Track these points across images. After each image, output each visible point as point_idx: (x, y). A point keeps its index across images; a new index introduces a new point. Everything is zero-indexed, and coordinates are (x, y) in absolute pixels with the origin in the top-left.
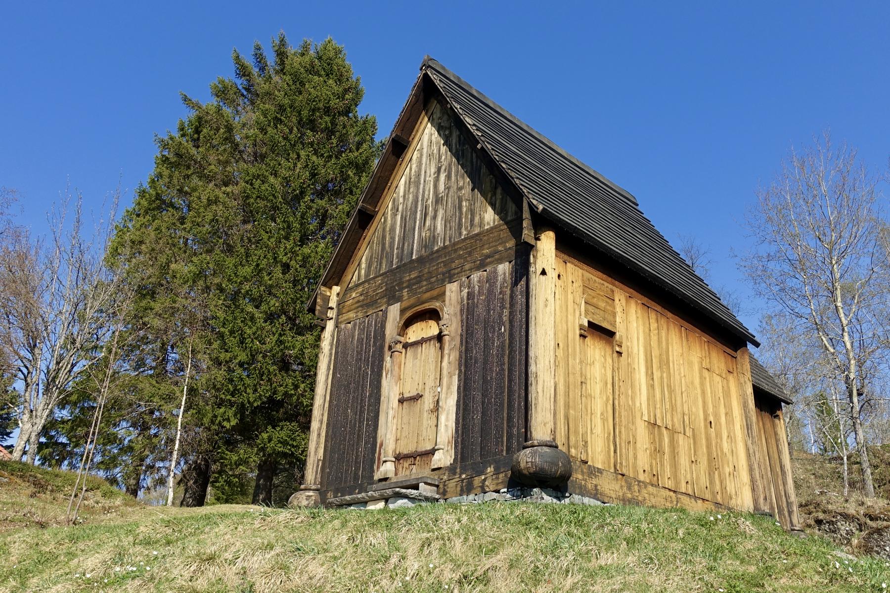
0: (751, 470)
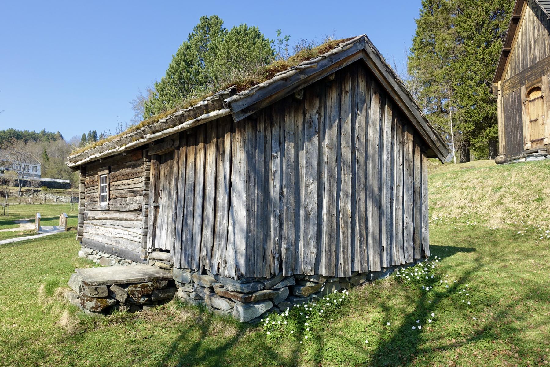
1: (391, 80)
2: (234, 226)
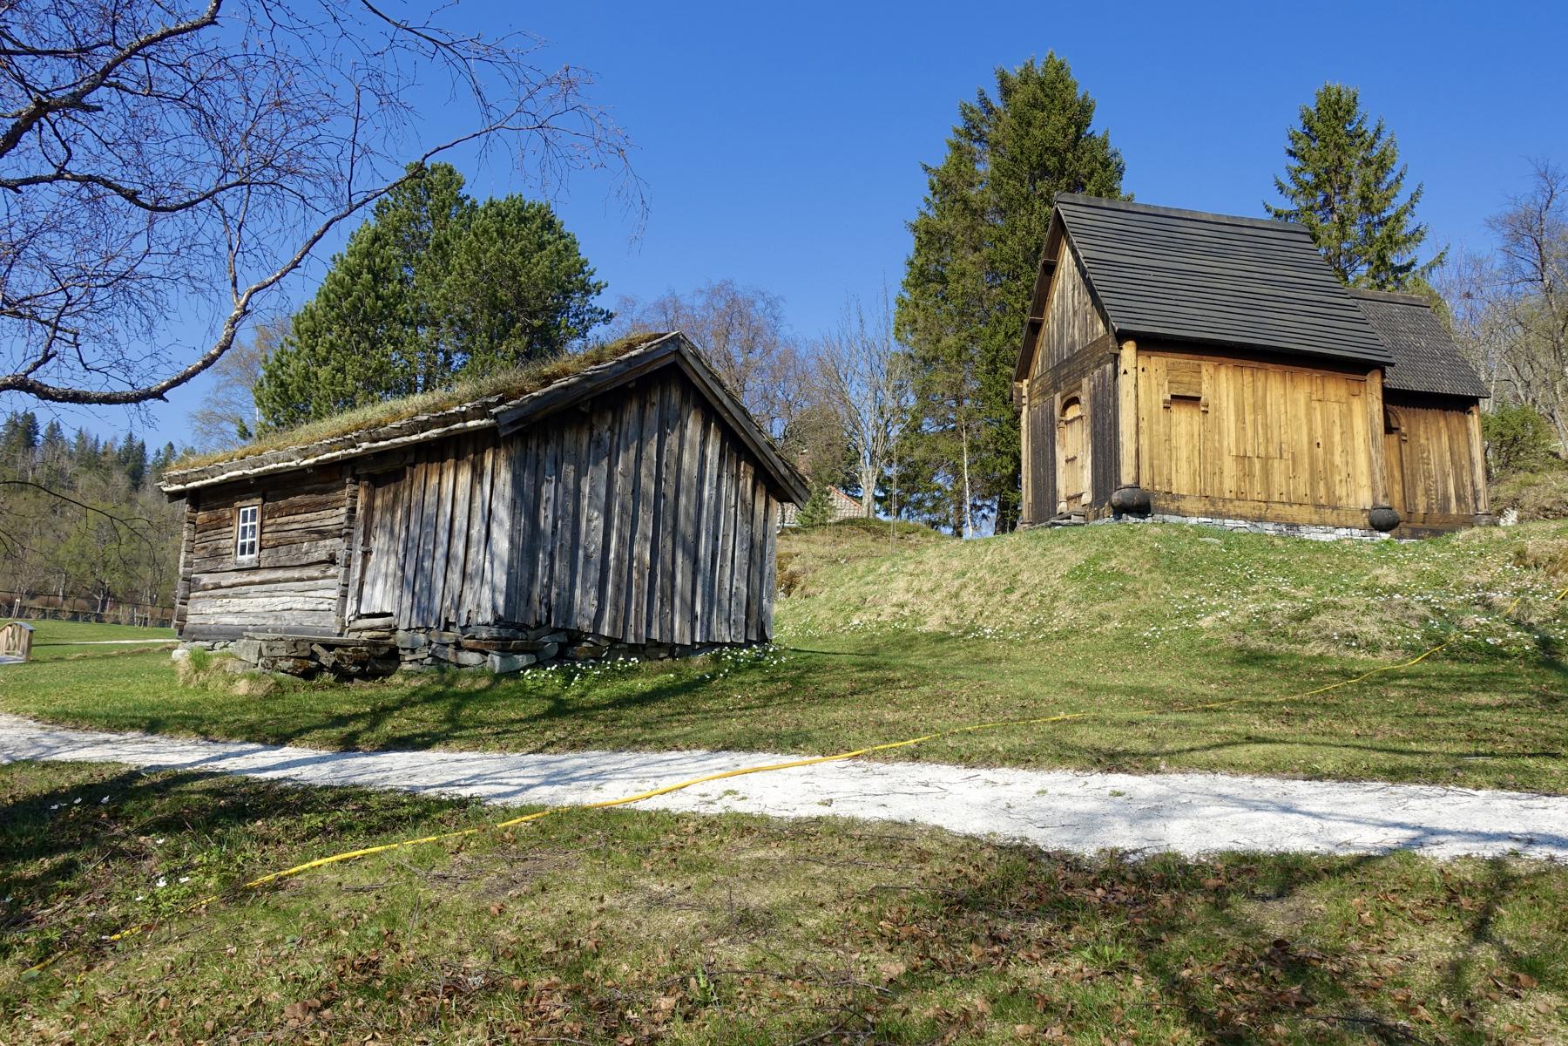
0: (1372, 474)
1: (718, 391)
2: (492, 563)
